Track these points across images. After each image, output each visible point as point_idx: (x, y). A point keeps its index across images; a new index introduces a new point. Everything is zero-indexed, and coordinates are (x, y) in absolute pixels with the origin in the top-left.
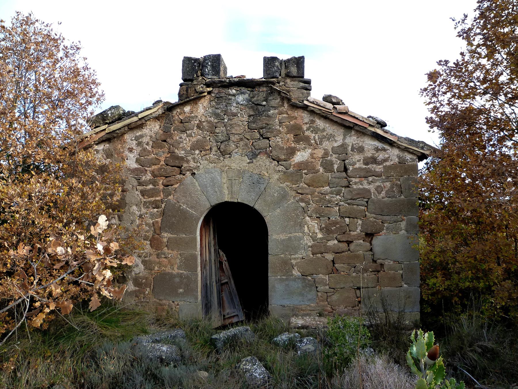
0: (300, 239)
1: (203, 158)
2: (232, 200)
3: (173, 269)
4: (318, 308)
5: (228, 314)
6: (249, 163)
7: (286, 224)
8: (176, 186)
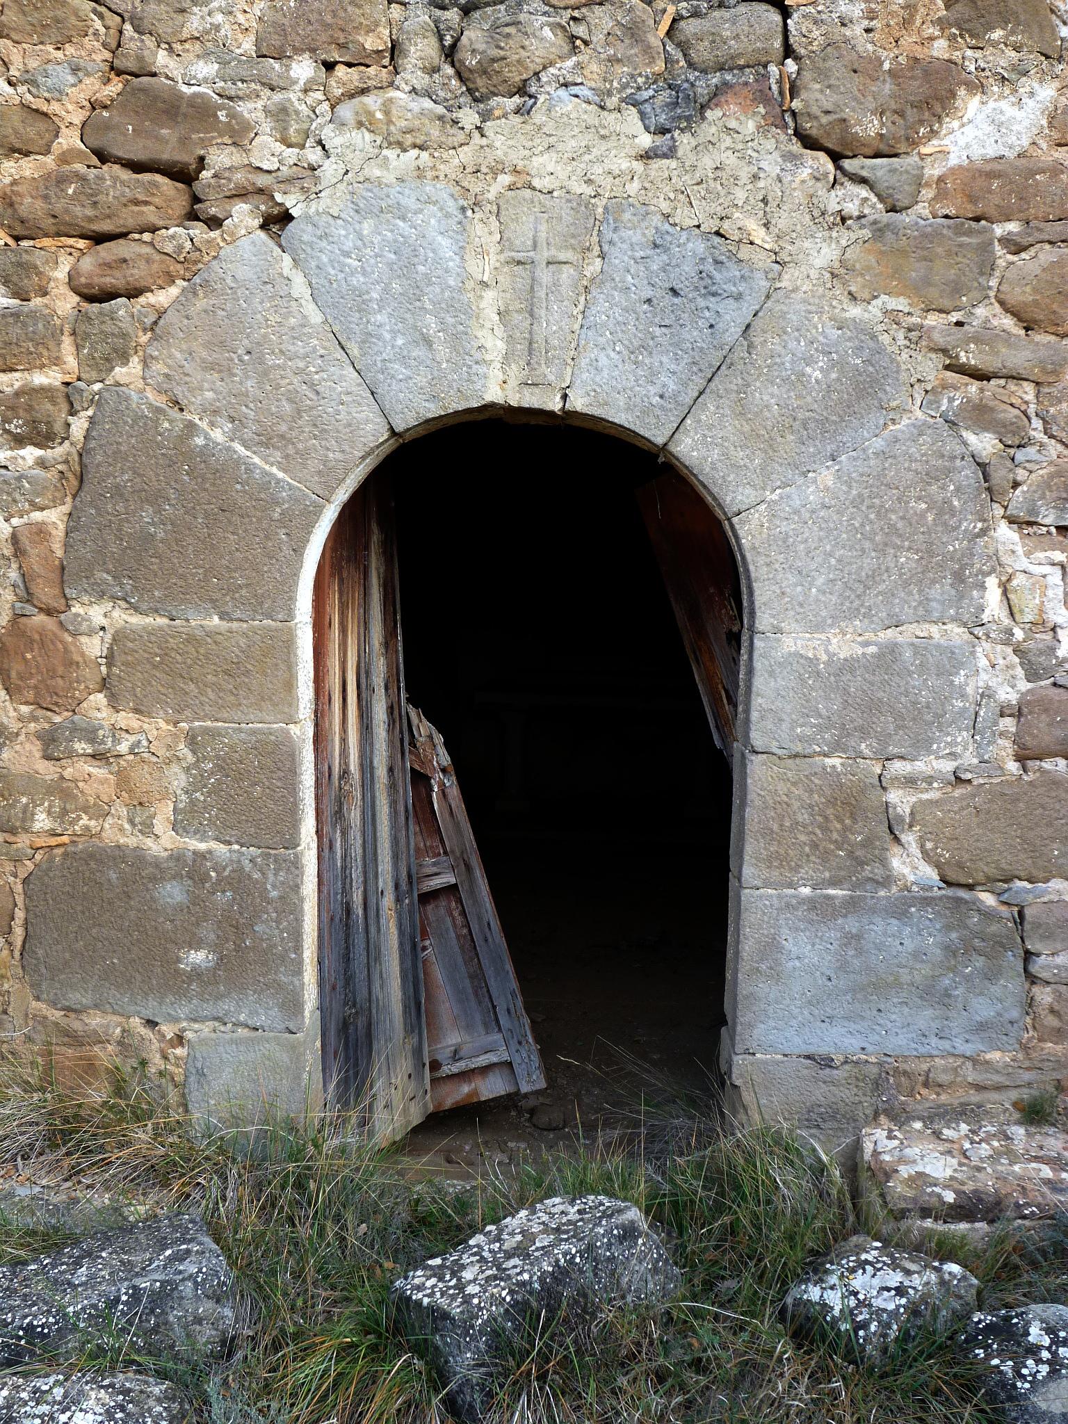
0: (953, 660)
1: (346, 111)
2: (531, 400)
3: (147, 828)
4: (1027, 1076)
5: (456, 1056)
7: (869, 562)
8: (162, 298)
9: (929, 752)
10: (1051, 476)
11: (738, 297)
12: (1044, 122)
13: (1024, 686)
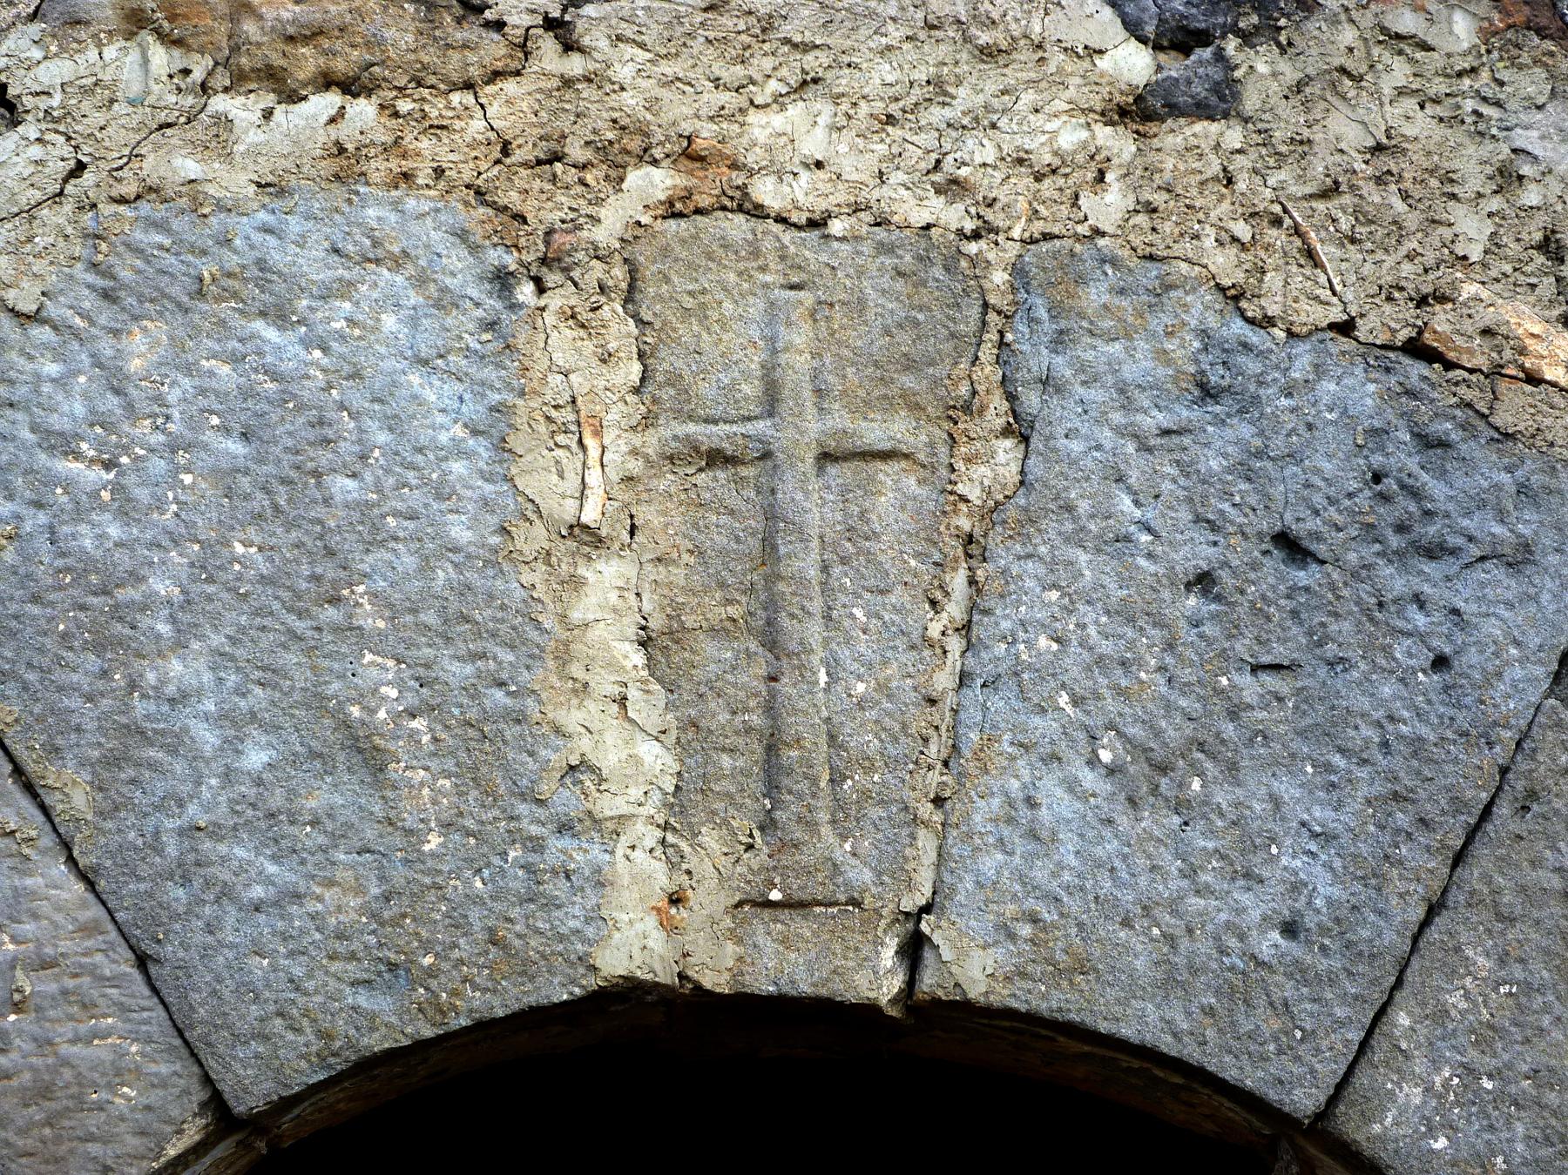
2: (783, 963)
6: (1138, 111)
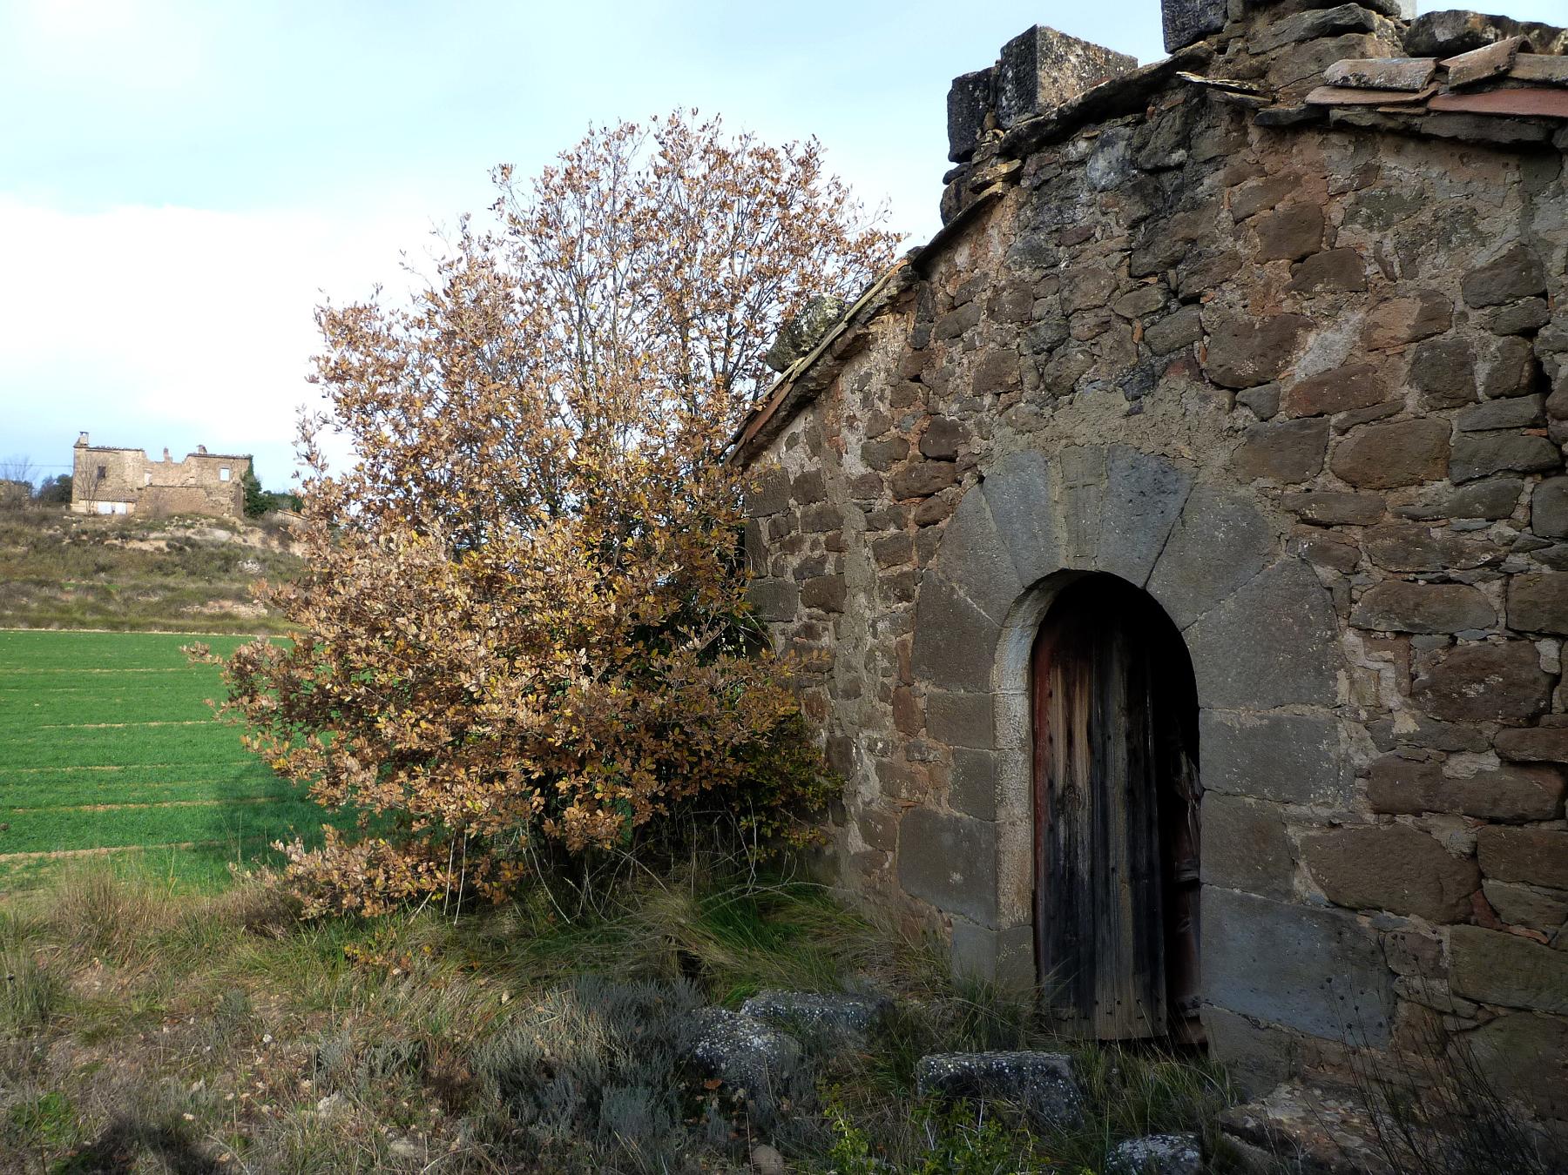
9: (1310, 800)
10: (1377, 594)
11: (1176, 492)
12: (1357, 338)
13: (1376, 755)
